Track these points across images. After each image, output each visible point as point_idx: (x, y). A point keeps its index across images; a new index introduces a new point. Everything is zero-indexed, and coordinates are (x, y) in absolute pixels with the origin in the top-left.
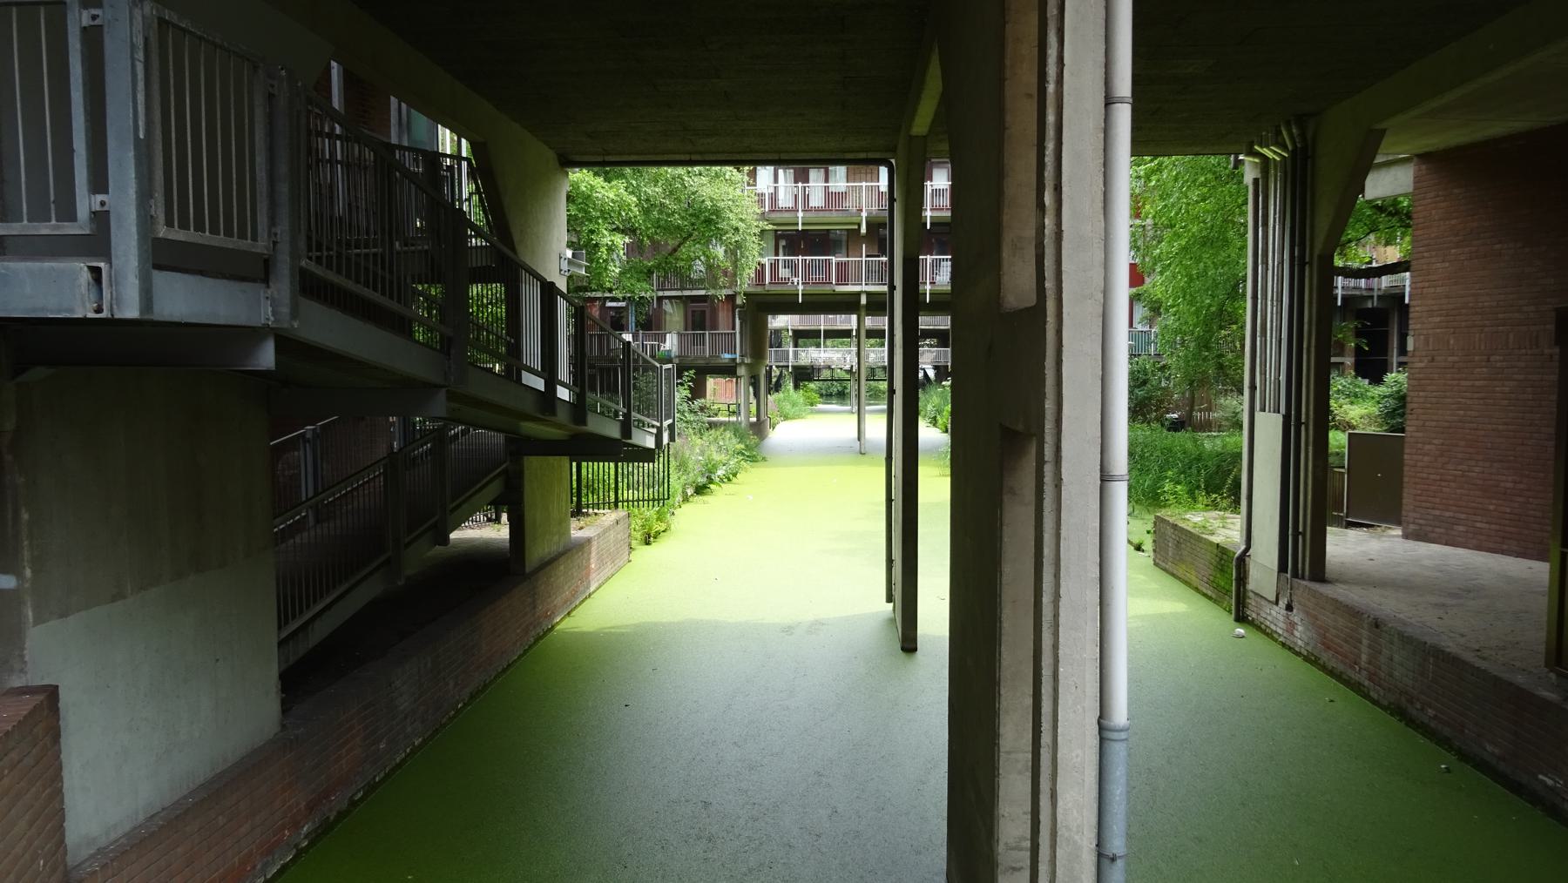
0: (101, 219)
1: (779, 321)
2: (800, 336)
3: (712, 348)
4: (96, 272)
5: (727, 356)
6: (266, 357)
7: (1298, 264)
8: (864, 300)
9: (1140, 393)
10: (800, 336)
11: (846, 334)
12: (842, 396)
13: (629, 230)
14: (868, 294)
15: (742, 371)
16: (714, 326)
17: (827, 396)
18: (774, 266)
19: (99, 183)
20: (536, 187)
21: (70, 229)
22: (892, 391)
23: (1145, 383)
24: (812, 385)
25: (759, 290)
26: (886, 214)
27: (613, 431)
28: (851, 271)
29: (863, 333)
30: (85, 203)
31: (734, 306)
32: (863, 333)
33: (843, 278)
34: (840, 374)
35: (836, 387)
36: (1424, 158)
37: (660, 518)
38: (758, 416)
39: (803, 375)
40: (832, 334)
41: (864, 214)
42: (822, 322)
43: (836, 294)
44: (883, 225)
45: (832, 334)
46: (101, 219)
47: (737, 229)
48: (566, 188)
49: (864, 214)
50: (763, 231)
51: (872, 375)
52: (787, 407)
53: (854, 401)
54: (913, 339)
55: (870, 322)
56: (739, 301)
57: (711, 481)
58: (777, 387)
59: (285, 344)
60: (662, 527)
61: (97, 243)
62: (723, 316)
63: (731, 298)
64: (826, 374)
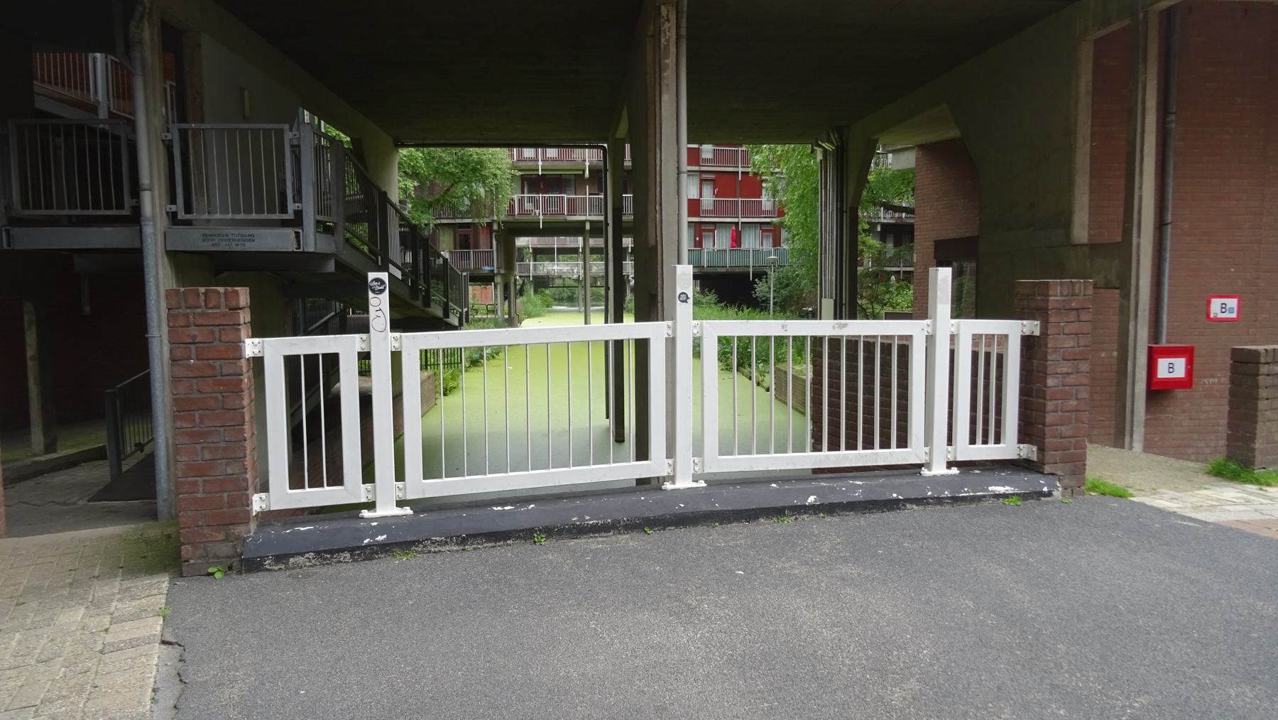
0: (299, 214)
1: (521, 242)
2: (539, 253)
3: (475, 263)
4: (297, 234)
5: (487, 268)
6: (331, 267)
7: (840, 212)
8: (588, 227)
9: (784, 292)
10: (539, 253)
11: (575, 251)
12: (571, 300)
13: (415, 175)
14: (591, 222)
15: (498, 279)
16: (477, 246)
17: (560, 300)
18: (521, 201)
19: (298, 197)
20: (384, 160)
21: (285, 217)
22: (607, 289)
23: (787, 285)
24: (547, 292)
25: (510, 219)
26: (602, 163)
27: (439, 312)
28: (578, 204)
29: (588, 251)
30: (292, 207)
31: (491, 231)
32: (588, 251)
33: (572, 211)
34: (569, 282)
35: (567, 293)
36: (921, 147)
37: (454, 378)
38: (509, 314)
39: (541, 283)
40: (562, 251)
41: (587, 164)
42: (556, 242)
43: (567, 222)
44: (600, 171)
45: (562, 251)
46: (299, 214)
47: (495, 175)
48: (398, 160)
49: (587, 164)
50: (513, 176)
51: (595, 279)
52: (531, 308)
53: (581, 303)
54: (620, 254)
55: (593, 242)
56: (495, 227)
57: (482, 357)
58: (521, 292)
59: (339, 265)
60: (455, 384)
61: (297, 221)
62: (483, 239)
63: (490, 225)
64: (558, 282)
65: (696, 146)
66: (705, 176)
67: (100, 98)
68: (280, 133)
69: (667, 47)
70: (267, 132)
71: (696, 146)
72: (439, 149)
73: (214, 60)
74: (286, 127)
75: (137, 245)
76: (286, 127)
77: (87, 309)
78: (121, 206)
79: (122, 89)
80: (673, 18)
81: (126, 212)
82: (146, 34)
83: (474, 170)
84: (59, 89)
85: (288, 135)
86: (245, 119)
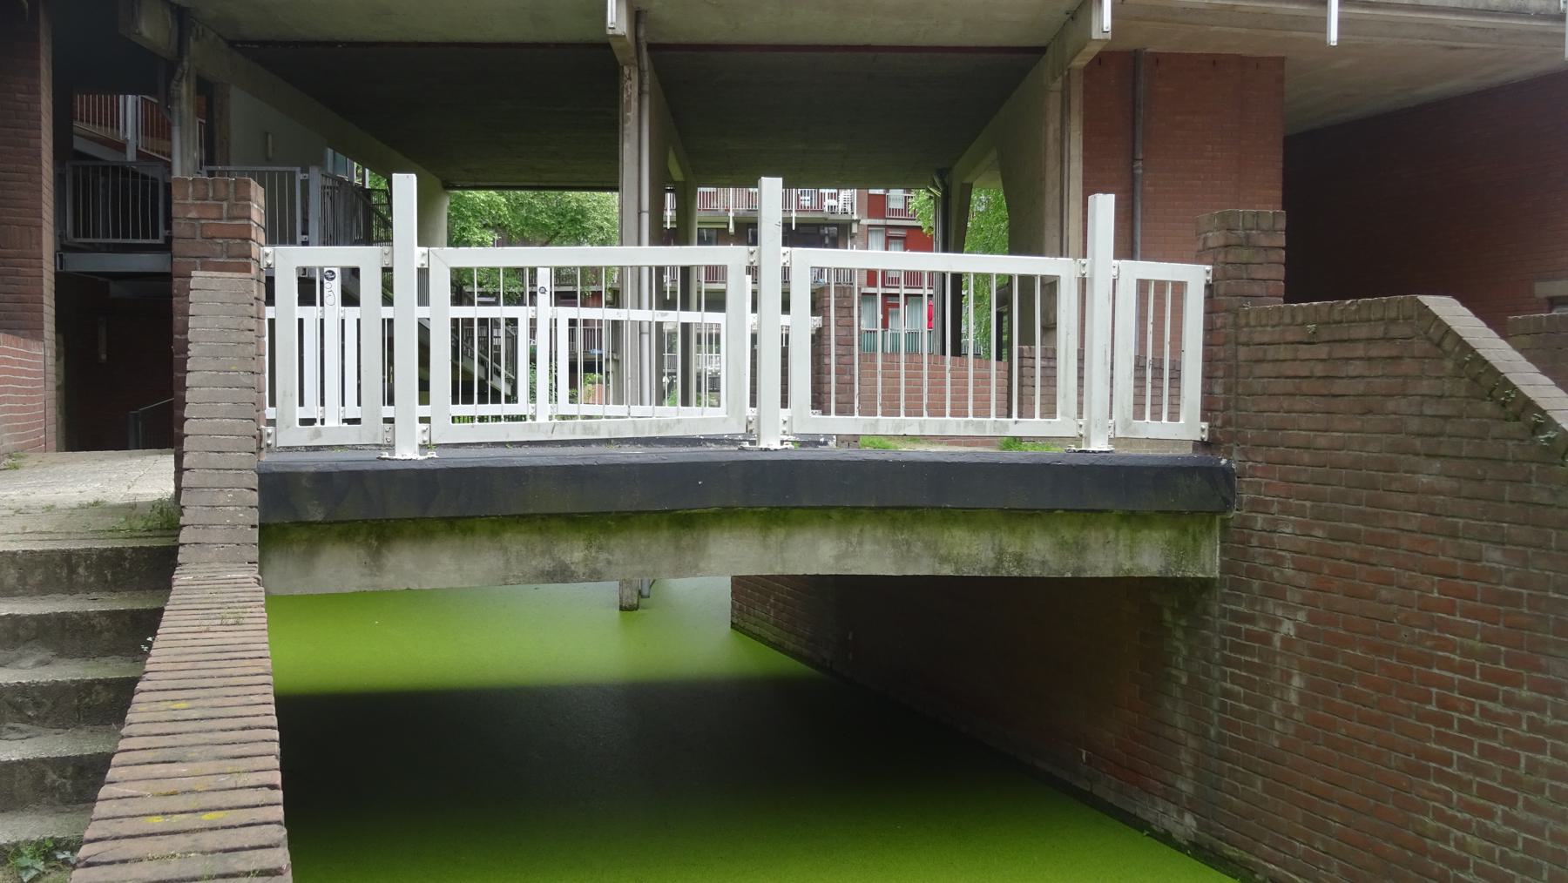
41: (731, 214)
47: (601, 228)
49: (731, 214)
65: (880, 192)
66: (892, 233)
67: (129, 136)
68: (292, 175)
69: (629, 102)
70: (281, 174)
71: (880, 192)
72: (529, 193)
73: (243, 110)
74: (298, 169)
75: (168, 270)
76: (298, 169)
77: (104, 357)
78: (156, 236)
79: (157, 126)
80: (635, 77)
81: (160, 241)
82: (184, 90)
83: (574, 221)
84: (90, 128)
85: (300, 177)
86: (268, 161)
